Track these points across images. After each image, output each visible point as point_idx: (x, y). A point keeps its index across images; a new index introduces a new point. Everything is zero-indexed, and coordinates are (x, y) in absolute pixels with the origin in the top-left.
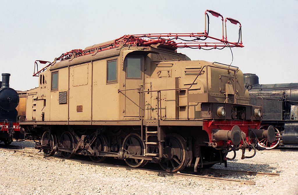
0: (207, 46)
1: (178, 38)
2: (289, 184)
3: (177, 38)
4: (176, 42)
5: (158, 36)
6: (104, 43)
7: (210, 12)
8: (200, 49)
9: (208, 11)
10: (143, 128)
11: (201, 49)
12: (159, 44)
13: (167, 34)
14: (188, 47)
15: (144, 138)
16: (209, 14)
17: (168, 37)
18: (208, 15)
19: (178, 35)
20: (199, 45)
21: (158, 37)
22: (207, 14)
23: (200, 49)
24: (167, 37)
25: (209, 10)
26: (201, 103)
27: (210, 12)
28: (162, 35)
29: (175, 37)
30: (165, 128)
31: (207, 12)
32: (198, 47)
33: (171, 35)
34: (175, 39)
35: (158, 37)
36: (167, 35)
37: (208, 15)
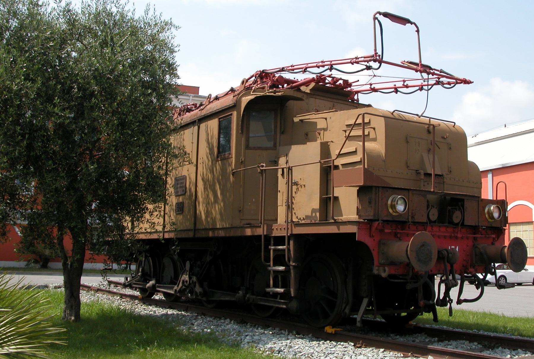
0: (407, 87)
1: (306, 72)
2: (51, 13)
3: (331, 69)
4: (350, 81)
5: (303, 68)
6: (496, 316)
7: (386, 15)
8: (397, 93)
9: (380, 13)
10: (261, 244)
11: (398, 93)
12: (313, 85)
13: (350, 60)
14: (377, 91)
15: (268, 260)
16: (381, 18)
17: (318, 67)
18: (379, 21)
19: (333, 62)
20: (395, 85)
21: (301, 70)
22: (377, 18)
23: (397, 93)
24: (317, 68)
25: (382, 11)
26: (358, 188)
27: (386, 15)
28: (309, 65)
29: (326, 67)
30: (299, 238)
31: (376, 16)
32: (393, 90)
33: (295, 67)
34: (302, 73)
35: (301, 70)
36: (315, 64)
37: (379, 21)
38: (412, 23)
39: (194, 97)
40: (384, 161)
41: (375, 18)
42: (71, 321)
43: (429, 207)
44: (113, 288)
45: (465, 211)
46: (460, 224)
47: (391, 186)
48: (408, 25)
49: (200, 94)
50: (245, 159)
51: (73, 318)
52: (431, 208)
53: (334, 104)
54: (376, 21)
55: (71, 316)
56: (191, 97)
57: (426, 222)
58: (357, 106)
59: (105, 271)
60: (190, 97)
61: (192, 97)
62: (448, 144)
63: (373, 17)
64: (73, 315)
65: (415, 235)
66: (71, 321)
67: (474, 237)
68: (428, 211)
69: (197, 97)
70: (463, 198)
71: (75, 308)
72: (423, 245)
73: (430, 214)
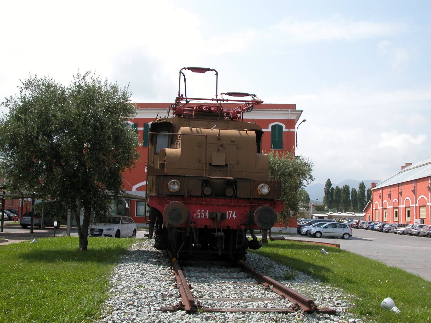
38: (212, 70)
39: (292, 111)
40: (180, 159)
41: (181, 72)
42: (80, 250)
43: (203, 186)
44: (280, 236)
45: (237, 188)
46: (233, 197)
47: (168, 175)
48: (207, 72)
49: (296, 109)
50: (153, 160)
51: (82, 249)
52: (205, 187)
53: (209, 123)
54: (181, 74)
55: (81, 248)
56: (290, 112)
57: (200, 195)
58: (228, 122)
59: (319, 225)
60: (289, 111)
61: (290, 111)
62: (236, 145)
63: (179, 71)
64: (82, 247)
65: (169, 203)
66: (80, 250)
67: (252, 206)
68: (202, 189)
69: (294, 111)
70: (6, 186)
71: (83, 244)
72: (174, 210)
73: (204, 191)
